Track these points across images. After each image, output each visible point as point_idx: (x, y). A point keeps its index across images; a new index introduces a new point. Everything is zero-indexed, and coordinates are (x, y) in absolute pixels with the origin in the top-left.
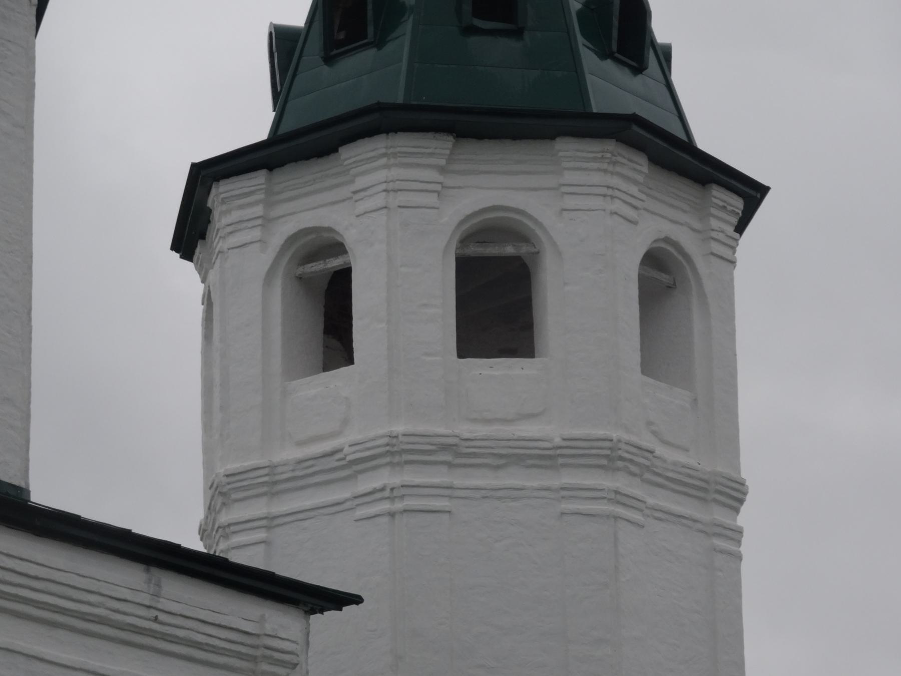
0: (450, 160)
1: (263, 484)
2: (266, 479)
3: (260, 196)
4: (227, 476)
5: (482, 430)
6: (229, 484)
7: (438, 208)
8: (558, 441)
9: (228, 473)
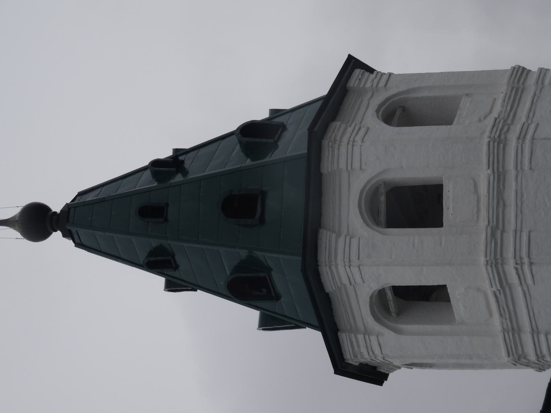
1: (513, 335)
2: (511, 334)
5: (484, 214)
6: (513, 355)
8: (490, 171)
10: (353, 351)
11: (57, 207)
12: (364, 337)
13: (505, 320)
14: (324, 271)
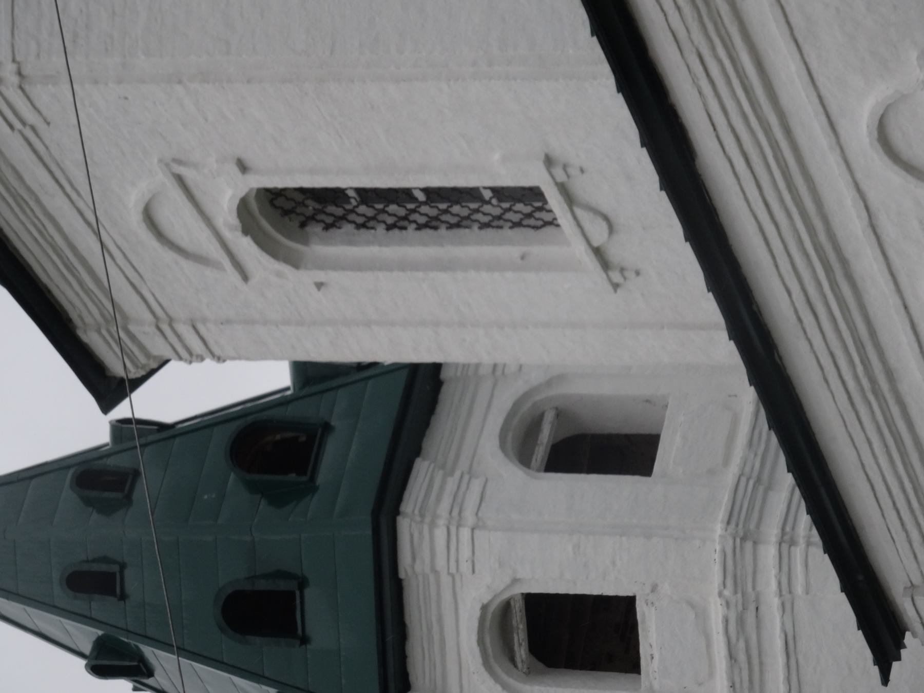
0: (443, 467)
1: (755, 488)
2: (751, 483)
3: (439, 475)
4: (728, 523)
6: (737, 525)
7: (487, 480)
9: (726, 520)
10: (423, 501)
13: (752, 456)
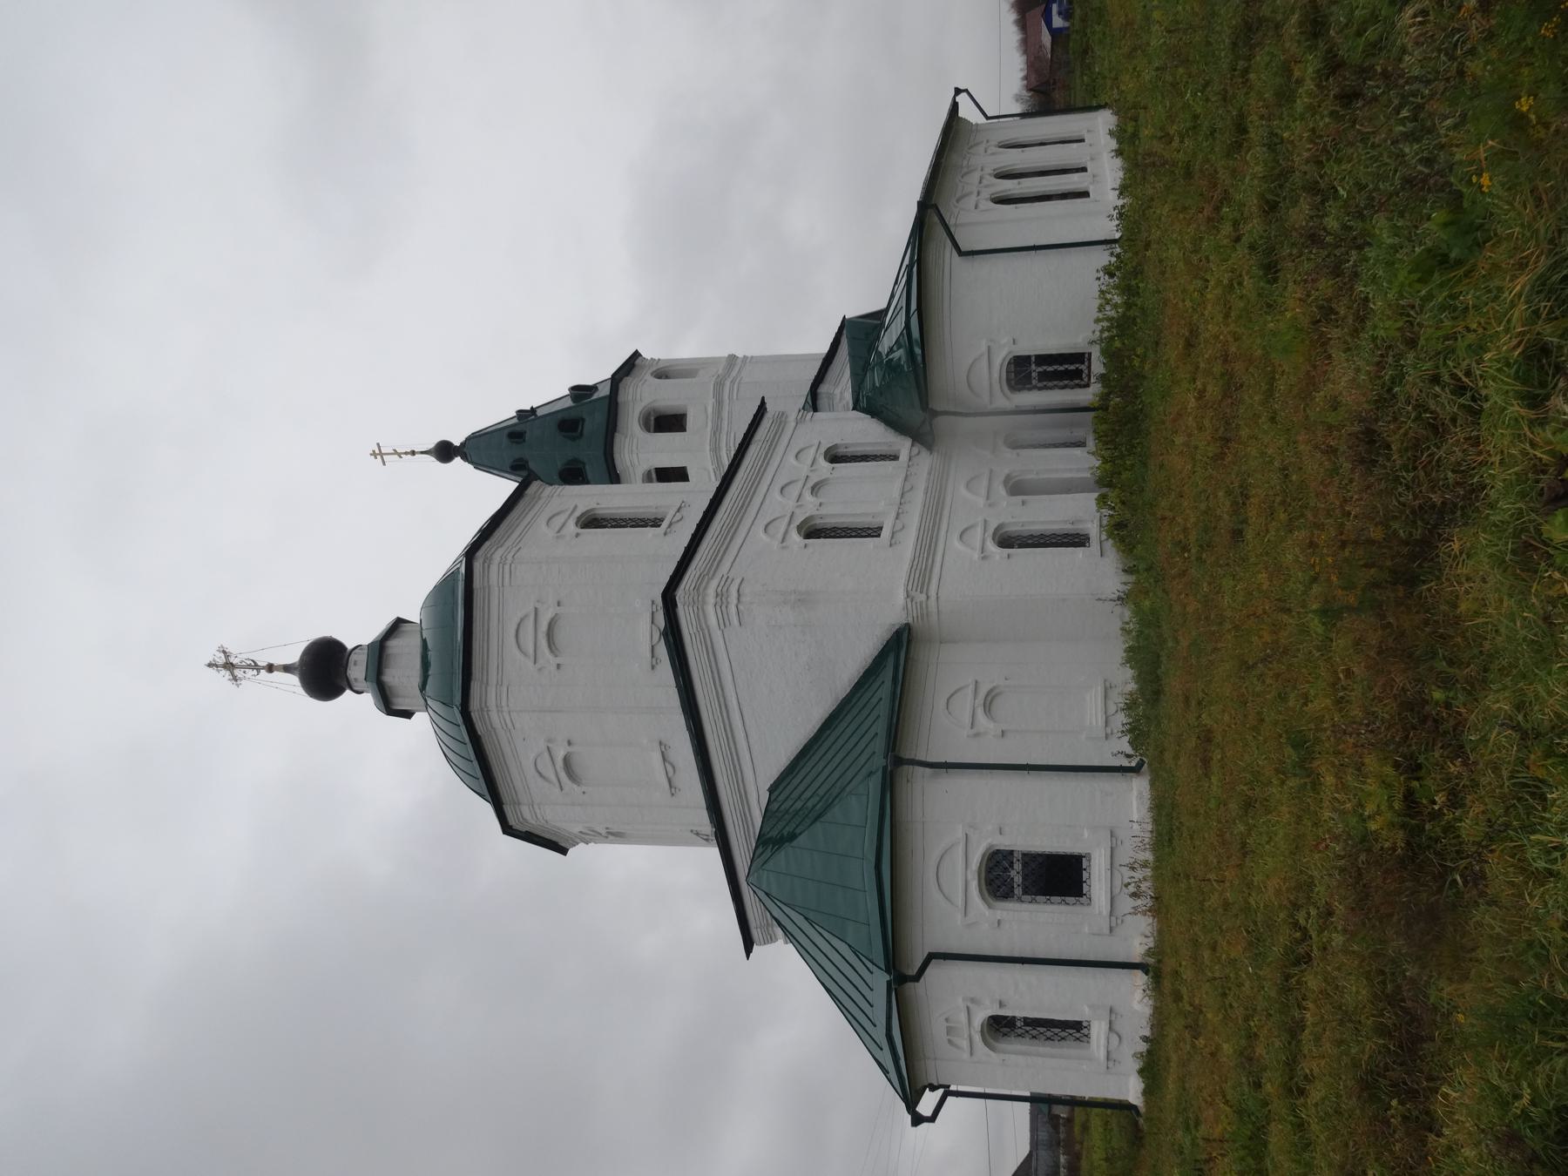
5: (710, 424)
8: (714, 400)
11: (457, 443)
12: (800, 834)
14: (616, 456)
